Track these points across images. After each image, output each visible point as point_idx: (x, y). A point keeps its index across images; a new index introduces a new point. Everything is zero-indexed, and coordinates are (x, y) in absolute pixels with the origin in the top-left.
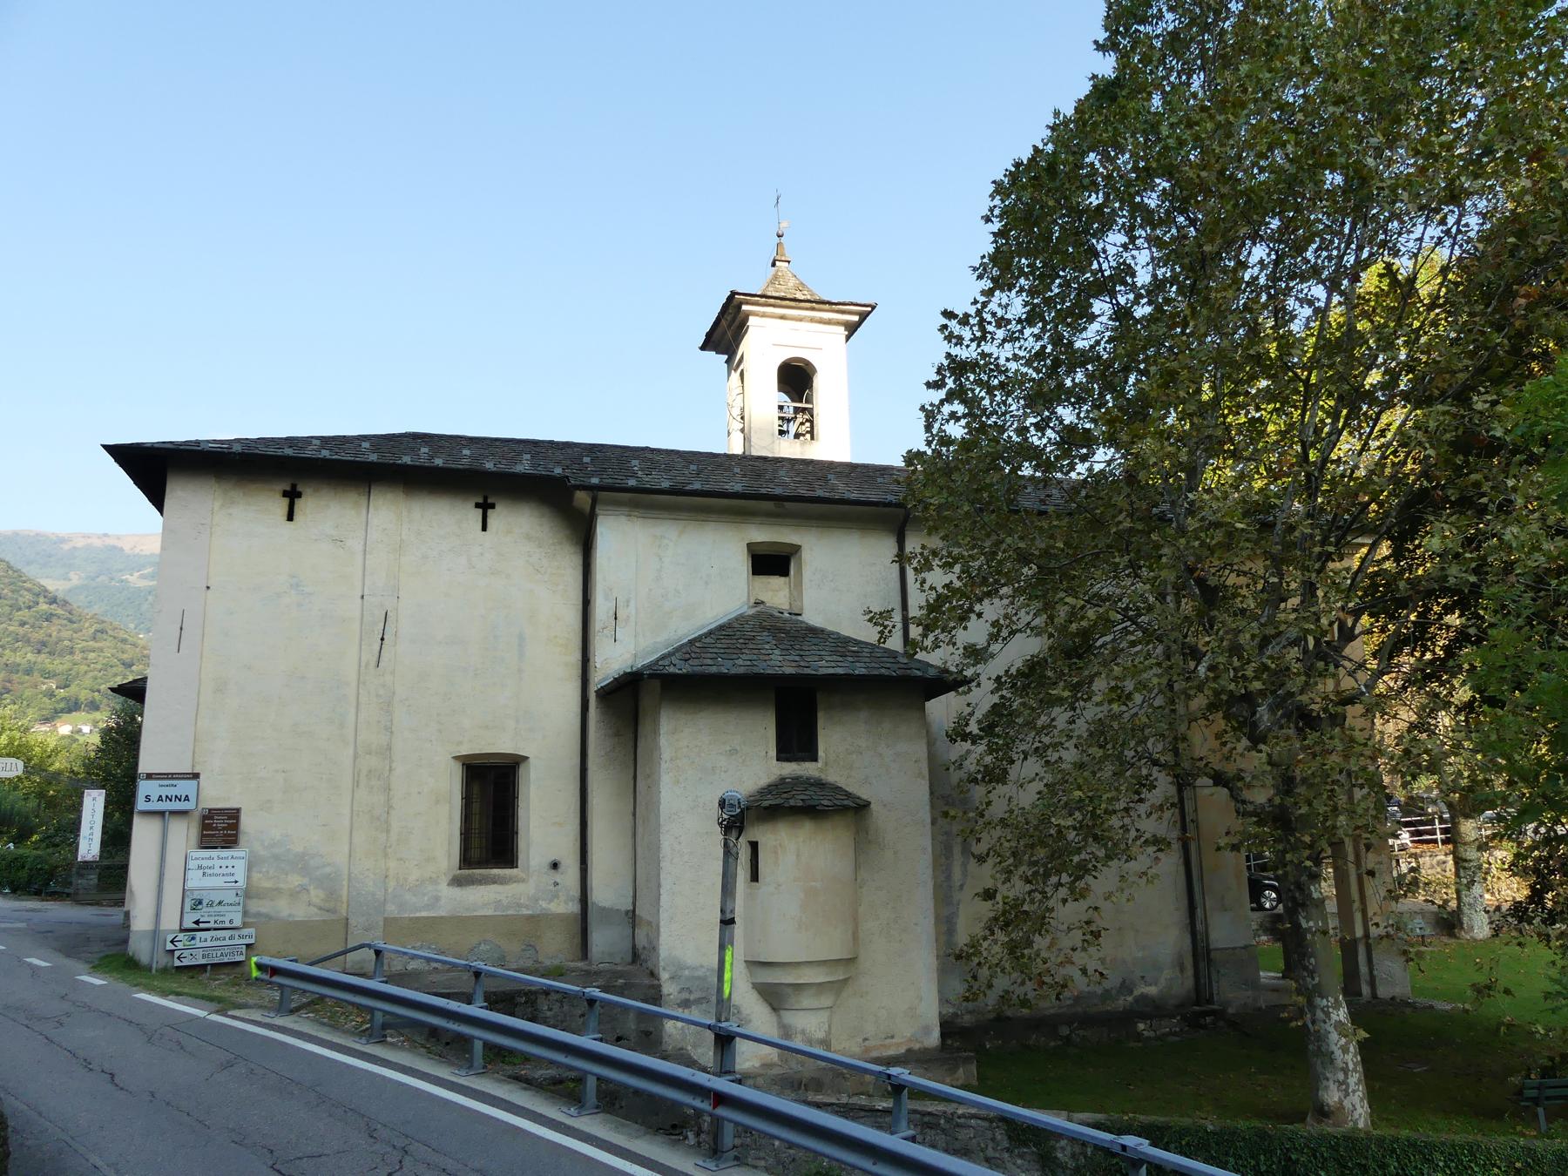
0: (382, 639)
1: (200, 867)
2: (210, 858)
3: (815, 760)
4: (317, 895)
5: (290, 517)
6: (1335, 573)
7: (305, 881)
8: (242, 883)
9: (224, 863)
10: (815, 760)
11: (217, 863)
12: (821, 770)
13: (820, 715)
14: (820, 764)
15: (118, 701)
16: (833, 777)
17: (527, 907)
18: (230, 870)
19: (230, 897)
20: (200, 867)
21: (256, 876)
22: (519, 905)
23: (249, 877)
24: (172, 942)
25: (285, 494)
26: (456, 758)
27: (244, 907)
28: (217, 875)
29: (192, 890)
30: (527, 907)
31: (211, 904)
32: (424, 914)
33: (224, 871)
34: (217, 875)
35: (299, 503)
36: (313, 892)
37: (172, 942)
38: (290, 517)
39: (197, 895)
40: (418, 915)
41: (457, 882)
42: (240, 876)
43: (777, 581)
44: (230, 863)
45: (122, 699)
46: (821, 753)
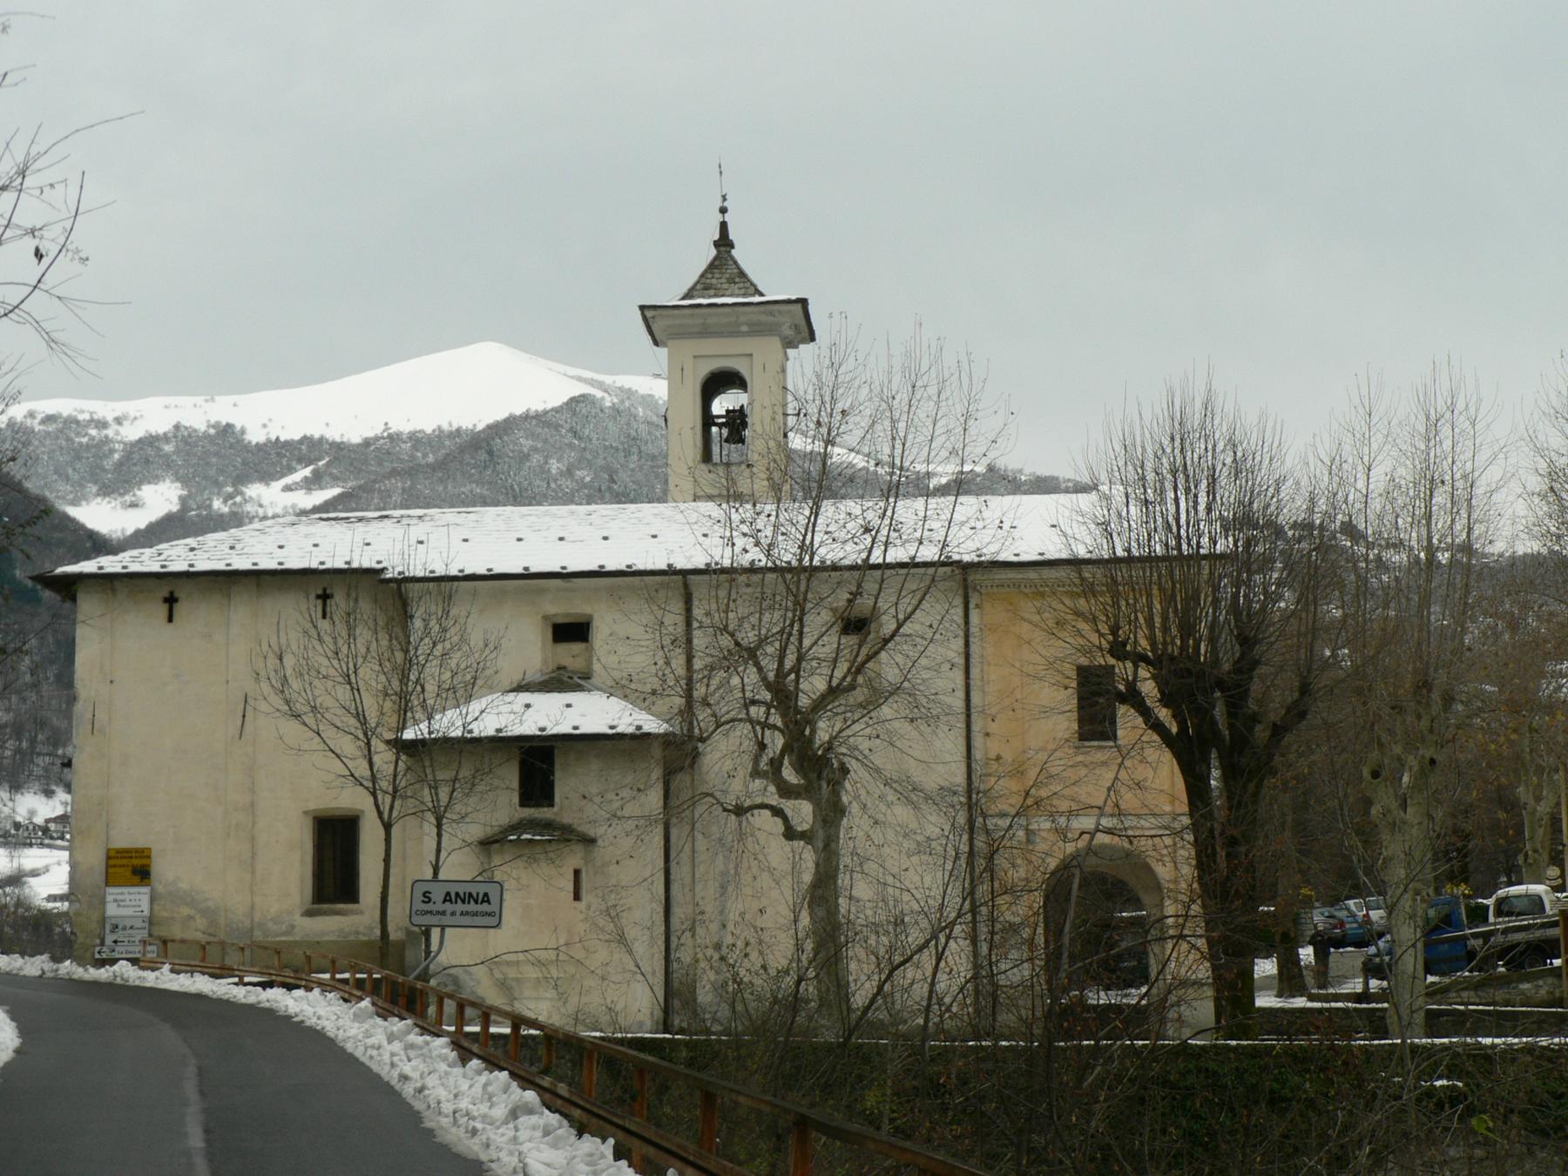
0: (244, 716)
1: (115, 901)
2: (122, 894)
3: (552, 805)
4: (200, 922)
5: (170, 619)
6: (1095, 620)
7: (193, 912)
8: (146, 913)
9: (133, 897)
10: (552, 805)
11: (127, 897)
12: (556, 814)
13: (557, 766)
14: (555, 809)
15: (339, 602)
16: (566, 819)
17: (364, 934)
18: (138, 902)
19: (138, 923)
20: (115, 901)
21: (156, 907)
22: (357, 933)
23: (151, 909)
24: (99, 952)
25: (166, 600)
26: (306, 813)
27: (149, 930)
28: (128, 906)
29: (110, 918)
30: (364, 934)
31: (124, 928)
32: (283, 938)
33: (133, 903)
34: (128, 906)
35: (177, 607)
36: (198, 921)
37: (99, 952)
38: (170, 619)
39: (114, 921)
40: (278, 939)
41: (309, 913)
42: (145, 906)
43: (577, 647)
44: (138, 897)
45: (78, 595)
46: (557, 799)
